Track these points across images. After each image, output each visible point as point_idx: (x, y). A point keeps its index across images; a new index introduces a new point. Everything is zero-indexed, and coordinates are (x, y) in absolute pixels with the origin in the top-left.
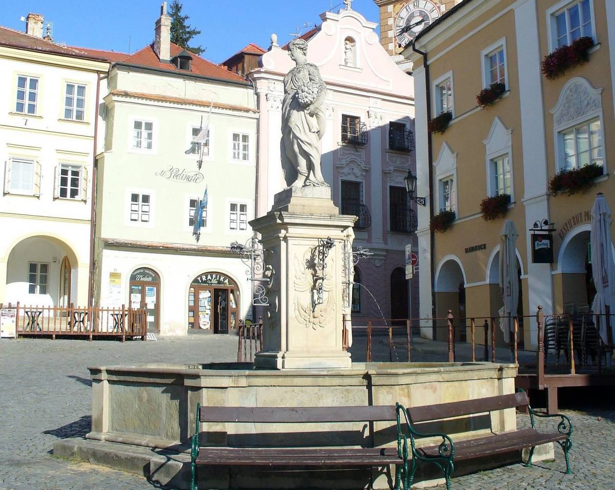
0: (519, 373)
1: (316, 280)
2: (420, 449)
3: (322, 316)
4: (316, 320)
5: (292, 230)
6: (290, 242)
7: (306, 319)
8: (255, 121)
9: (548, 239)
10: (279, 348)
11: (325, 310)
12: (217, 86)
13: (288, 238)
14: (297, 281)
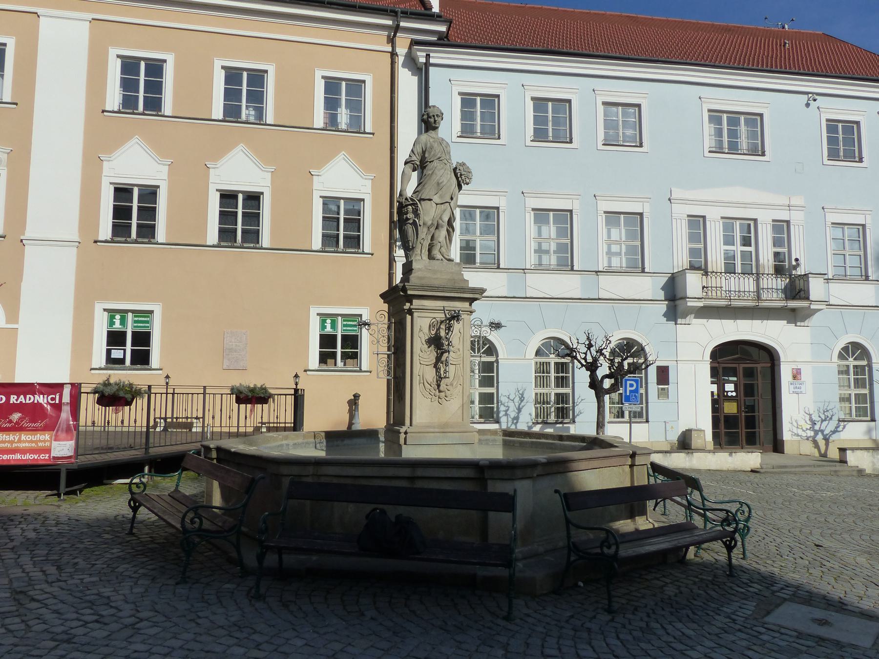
1: (442, 354)
4: (442, 394)
5: (416, 303)
6: (415, 314)
11: (452, 385)
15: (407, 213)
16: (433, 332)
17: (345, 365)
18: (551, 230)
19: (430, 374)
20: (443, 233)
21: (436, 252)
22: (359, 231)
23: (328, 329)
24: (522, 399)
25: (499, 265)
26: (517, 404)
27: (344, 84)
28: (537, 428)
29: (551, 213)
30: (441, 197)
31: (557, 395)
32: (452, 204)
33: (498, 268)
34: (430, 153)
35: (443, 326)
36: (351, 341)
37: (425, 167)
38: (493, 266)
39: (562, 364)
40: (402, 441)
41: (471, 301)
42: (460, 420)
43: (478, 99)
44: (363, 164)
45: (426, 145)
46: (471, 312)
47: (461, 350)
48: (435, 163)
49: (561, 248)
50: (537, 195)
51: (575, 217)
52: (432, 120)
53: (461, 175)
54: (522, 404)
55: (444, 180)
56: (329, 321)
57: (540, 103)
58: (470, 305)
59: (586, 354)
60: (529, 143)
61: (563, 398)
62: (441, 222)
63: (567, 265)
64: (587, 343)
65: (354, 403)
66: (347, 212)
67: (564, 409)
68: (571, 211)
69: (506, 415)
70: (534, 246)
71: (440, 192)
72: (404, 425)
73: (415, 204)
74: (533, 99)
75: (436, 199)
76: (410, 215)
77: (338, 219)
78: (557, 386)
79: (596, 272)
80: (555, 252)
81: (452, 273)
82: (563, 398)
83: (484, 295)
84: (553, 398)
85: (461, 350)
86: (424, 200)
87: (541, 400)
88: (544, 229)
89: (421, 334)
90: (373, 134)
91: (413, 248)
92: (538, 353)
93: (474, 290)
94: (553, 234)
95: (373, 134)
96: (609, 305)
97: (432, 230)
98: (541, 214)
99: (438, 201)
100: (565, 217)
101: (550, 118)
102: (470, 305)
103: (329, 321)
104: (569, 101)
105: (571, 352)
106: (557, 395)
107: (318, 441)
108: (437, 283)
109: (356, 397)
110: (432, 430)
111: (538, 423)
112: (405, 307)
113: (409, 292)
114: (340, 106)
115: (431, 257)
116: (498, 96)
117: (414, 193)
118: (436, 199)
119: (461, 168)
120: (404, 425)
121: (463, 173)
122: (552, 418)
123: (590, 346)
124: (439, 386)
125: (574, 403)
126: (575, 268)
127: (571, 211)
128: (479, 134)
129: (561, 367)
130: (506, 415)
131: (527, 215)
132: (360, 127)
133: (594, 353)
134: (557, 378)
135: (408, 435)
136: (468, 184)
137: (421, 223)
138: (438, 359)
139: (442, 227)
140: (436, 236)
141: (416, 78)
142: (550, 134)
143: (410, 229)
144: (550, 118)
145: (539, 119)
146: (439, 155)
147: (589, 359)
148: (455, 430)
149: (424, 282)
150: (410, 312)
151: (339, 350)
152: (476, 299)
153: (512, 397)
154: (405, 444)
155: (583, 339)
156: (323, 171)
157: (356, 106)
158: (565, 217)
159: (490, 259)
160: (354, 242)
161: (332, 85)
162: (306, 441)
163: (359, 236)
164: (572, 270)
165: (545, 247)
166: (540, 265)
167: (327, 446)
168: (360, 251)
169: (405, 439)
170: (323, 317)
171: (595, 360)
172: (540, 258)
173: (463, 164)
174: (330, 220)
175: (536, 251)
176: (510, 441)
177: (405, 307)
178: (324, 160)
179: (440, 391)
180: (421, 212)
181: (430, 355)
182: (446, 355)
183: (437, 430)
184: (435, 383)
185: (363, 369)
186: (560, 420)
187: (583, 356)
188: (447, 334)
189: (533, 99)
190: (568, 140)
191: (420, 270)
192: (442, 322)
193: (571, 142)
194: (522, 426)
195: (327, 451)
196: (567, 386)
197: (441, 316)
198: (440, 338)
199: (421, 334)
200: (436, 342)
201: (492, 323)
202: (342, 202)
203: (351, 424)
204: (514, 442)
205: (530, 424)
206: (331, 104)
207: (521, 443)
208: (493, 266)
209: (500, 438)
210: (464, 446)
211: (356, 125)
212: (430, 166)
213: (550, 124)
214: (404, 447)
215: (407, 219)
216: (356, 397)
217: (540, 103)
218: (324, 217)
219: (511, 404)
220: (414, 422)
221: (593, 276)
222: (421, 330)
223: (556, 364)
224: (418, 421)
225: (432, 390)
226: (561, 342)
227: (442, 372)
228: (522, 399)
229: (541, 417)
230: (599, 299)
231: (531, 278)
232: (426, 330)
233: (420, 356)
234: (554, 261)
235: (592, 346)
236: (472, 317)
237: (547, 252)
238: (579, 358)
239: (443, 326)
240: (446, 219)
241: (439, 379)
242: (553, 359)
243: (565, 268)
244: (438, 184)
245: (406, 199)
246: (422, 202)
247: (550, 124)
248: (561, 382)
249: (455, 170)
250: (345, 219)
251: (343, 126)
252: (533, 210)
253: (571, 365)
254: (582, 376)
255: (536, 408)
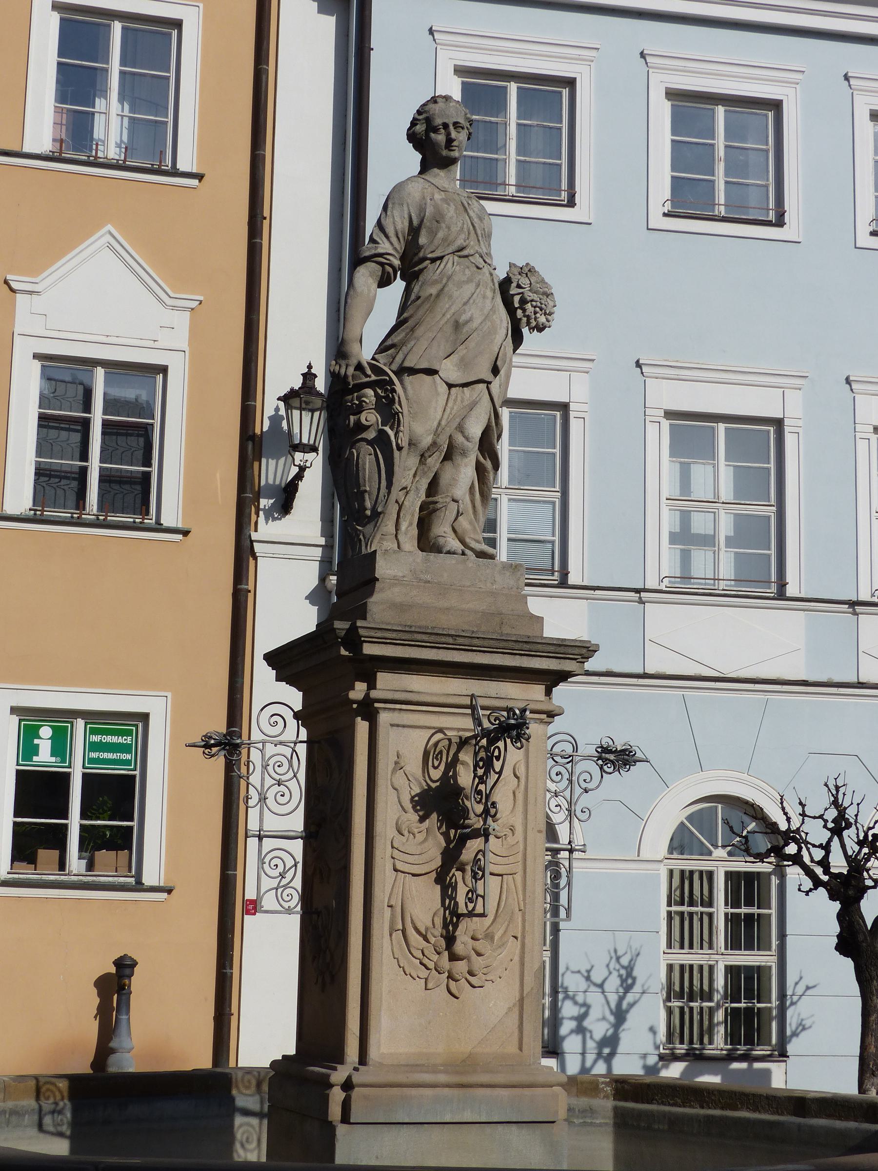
0: (109, 26)
1: (463, 840)
2: (550, 723)
3: (479, 954)
4: (461, 967)
5: (388, 683)
6: (384, 718)
7: (425, 961)
8: (453, 390)
9: (100, 226)
10: (339, 1058)
11: (489, 937)
12: (733, 568)
13: (376, 705)
14: (399, 841)
15: (359, 409)
16: (436, 774)
17: (90, 867)
18: (717, 477)
19: (425, 904)
20: (464, 474)
21: (442, 529)
22: (148, 462)
23: (45, 756)
24: (628, 982)
25: (565, 574)
26: (613, 999)
27: (117, 28)
28: (674, 1071)
29: (721, 427)
30: (464, 364)
31: (731, 970)
32: (495, 387)
33: (563, 583)
34: (433, 233)
35: (466, 757)
36: (115, 796)
37: (416, 276)
38: (545, 578)
39: (750, 877)
40: (335, 1111)
41: (552, 679)
42: (513, 1049)
43: (513, 88)
44: (166, 261)
45: (422, 210)
46: (551, 715)
47: (519, 829)
48: (450, 265)
49: (747, 531)
50: (678, 372)
51: (790, 441)
52: (440, 138)
53: (523, 301)
54: (630, 998)
55: (475, 314)
56: (46, 732)
57: (690, 104)
58: (548, 693)
59: (826, 848)
60: (658, 221)
61: (749, 979)
62: (459, 439)
63: (765, 581)
64: (832, 814)
65: (115, 986)
66: (110, 405)
67: (755, 1015)
68: (778, 424)
69: (580, 1030)
70: (669, 521)
71: (462, 351)
72: (341, 1061)
73: (384, 385)
74: (672, 94)
75: (450, 370)
76: (370, 417)
77: (86, 424)
78: (734, 944)
79: (853, 604)
80: (730, 542)
81: (493, 594)
82: (749, 979)
83: (589, 665)
84: (720, 981)
85: (519, 829)
86: (413, 371)
87: (684, 987)
88: (700, 473)
89: (400, 780)
90: (200, 177)
91: (376, 515)
92: (681, 843)
93: (564, 649)
94: (726, 491)
95: (200, 177)
96: (671, 694)
97: (434, 461)
98: (691, 429)
99: (455, 376)
100: (762, 438)
101: (721, 152)
102: (548, 693)
103: (46, 732)
104: (776, 106)
105: (780, 843)
106: (731, 970)
107: (47, 1105)
108: (449, 623)
109: (125, 966)
110: (427, 1078)
111: (675, 1058)
112: (353, 695)
113: (369, 649)
114: (104, 93)
115: (427, 542)
116: (570, 83)
117: (383, 348)
118: (450, 370)
119: (524, 281)
120: (341, 1061)
121: (529, 295)
122: (719, 1043)
123: (839, 826)
124: (450, 940)
125: (782, 996)
126: (791, 591)
127: (778, 424)
128: (512, 190)
129: (745, 888)
130: (580, 1030)
131: (652, 430)
132: (162, 153)
133: (852, 847)
134: (732, 920)
135: (356, 1093)
136: (540, 329)
137: (404, 441)
138: (451, 856)
139: (464, 453)
140: (444, 480)
141: (329, 22)
142: (721, 197)
143: (367, 459)
144: (721, 152)
145: (690, 157)
146: (460, 242)
147: (838, 864)
148: (500, 1079)
149: (409, 619)
150: (368, 710)
151: (75, 821)
152: (563, 676)
153: (597, 977)
154: (346, 1119)
155: (819, 803)
156: (45, 281)
157: (152, 95)
158: (762, 438)
159: (539, 557)
160: (131, 494)
161: (81, 33)
162: (10, 1104)
163: (147, 476)
164: (781, 595)
165: (700, 524)
166: (686, 577)
167: (75, 1124)
168: (150, 521)
169: (346, 1106)
170: (30, 718)
171: (856, 866)
172: (686, 559)
173: (528, 271)
174: (60, 427)
175: (674, 538)
176: (640, 1114)
177: (353, 695)
178: (54, 244)
179: (453, 957)
180: (404, 408)
181: (426, 844)
182: (473, 845)
183: (442, 1078)
184: (439, 930)
185: (149, 879)
186: (742, 1049)
187: (819, 854)
188: (482, 780)
189: (672, 94)
190: (772, 216)
191: (397, 581)
192: (463, 743)
193: (780, 222)
194: (627, 1065)
195: (75, 1140)
196: (763, 945)
197: (463, 724)
198: (458, 791)
199: (400, 780)
200: (443, 803)
201: (605, 750)
202: (100, 372)
203: (104, 1050)
204: (650, 1115)
205: (652, 1060)
206: (78, 85)
207: (674, 1122)
208: (545, 578)
209: (606, 1105)
210: (525, 1130)
211: (151, 153)
212: (432, 272)
213: (720, 168)
214: (341, 1130)
215: (361, 428)
216: (125, 966)
217: (690, 104)
218: (42, 418)
219: (594, 998)
220: (373, 1053)
221: (842, 617)
222: (398, 766)
223: (729, 875)
224: (384, 1050)
225: (430, 951)
226: (755, 812)
227: (461, 898)
228: (628, 982)
229: (685, 1035)
230: (861, 685)
231: (661, 618)
232: (414, 765)
233: (398, 848)
234: (727, 568)
235: (848, 826)
236: (551, 729)
237: (708, 541)
238: (806, 859)
239: (466, 757)
240: (476, 430)
241: (452, 918)
242: (721, 863)
243: (759, 590)
244: (457, 326)
245: (359, 367)
246: (407, 379)
247: (720, 168)
248: (746, 932)
249: (505, 285)
250: (106, 424)
251: (113, 152)
252: (670, 414)
253: (774, 881)
254: (811, 917)
255: (670, 1011)
